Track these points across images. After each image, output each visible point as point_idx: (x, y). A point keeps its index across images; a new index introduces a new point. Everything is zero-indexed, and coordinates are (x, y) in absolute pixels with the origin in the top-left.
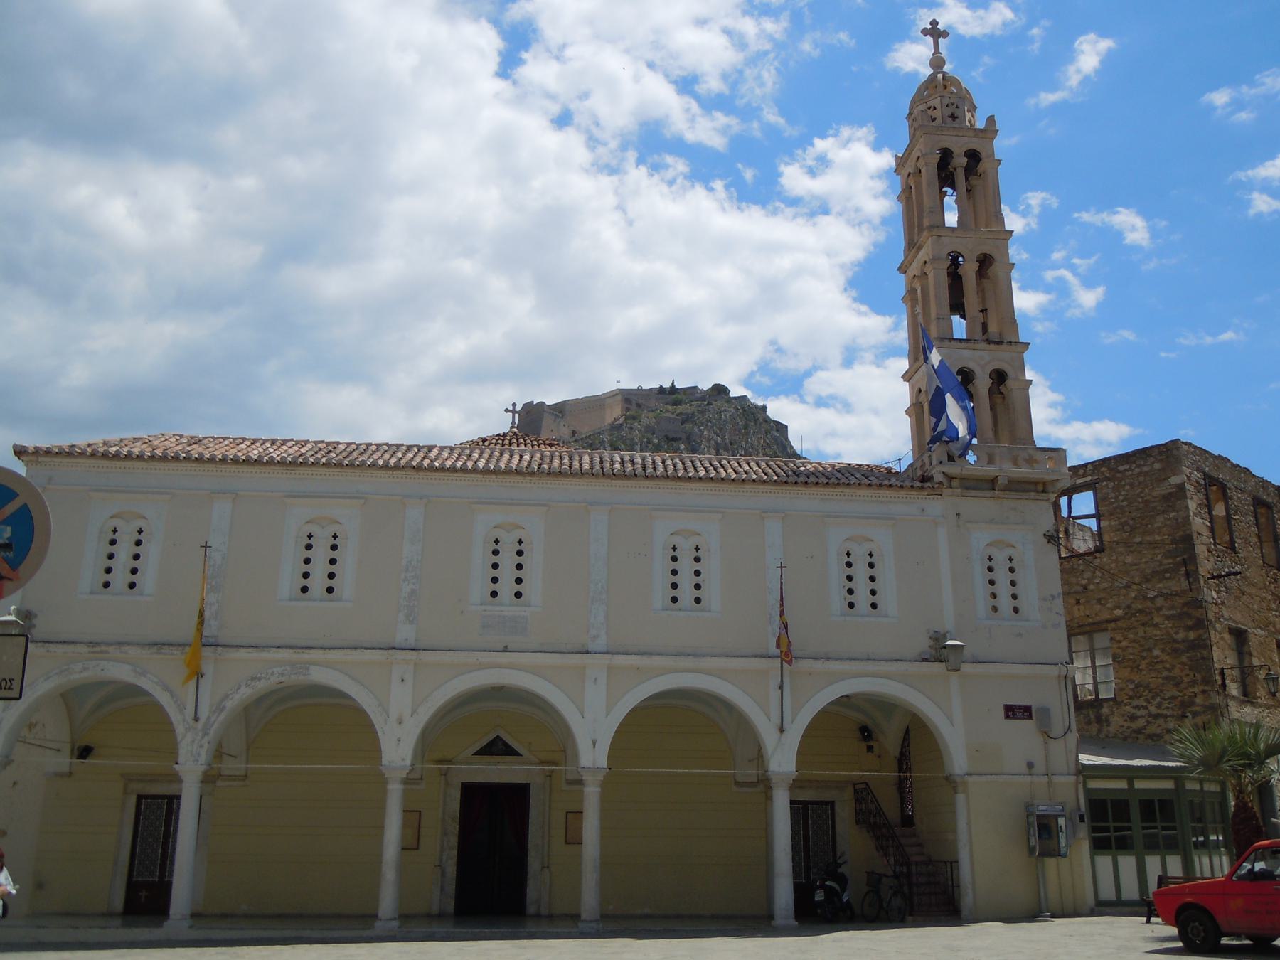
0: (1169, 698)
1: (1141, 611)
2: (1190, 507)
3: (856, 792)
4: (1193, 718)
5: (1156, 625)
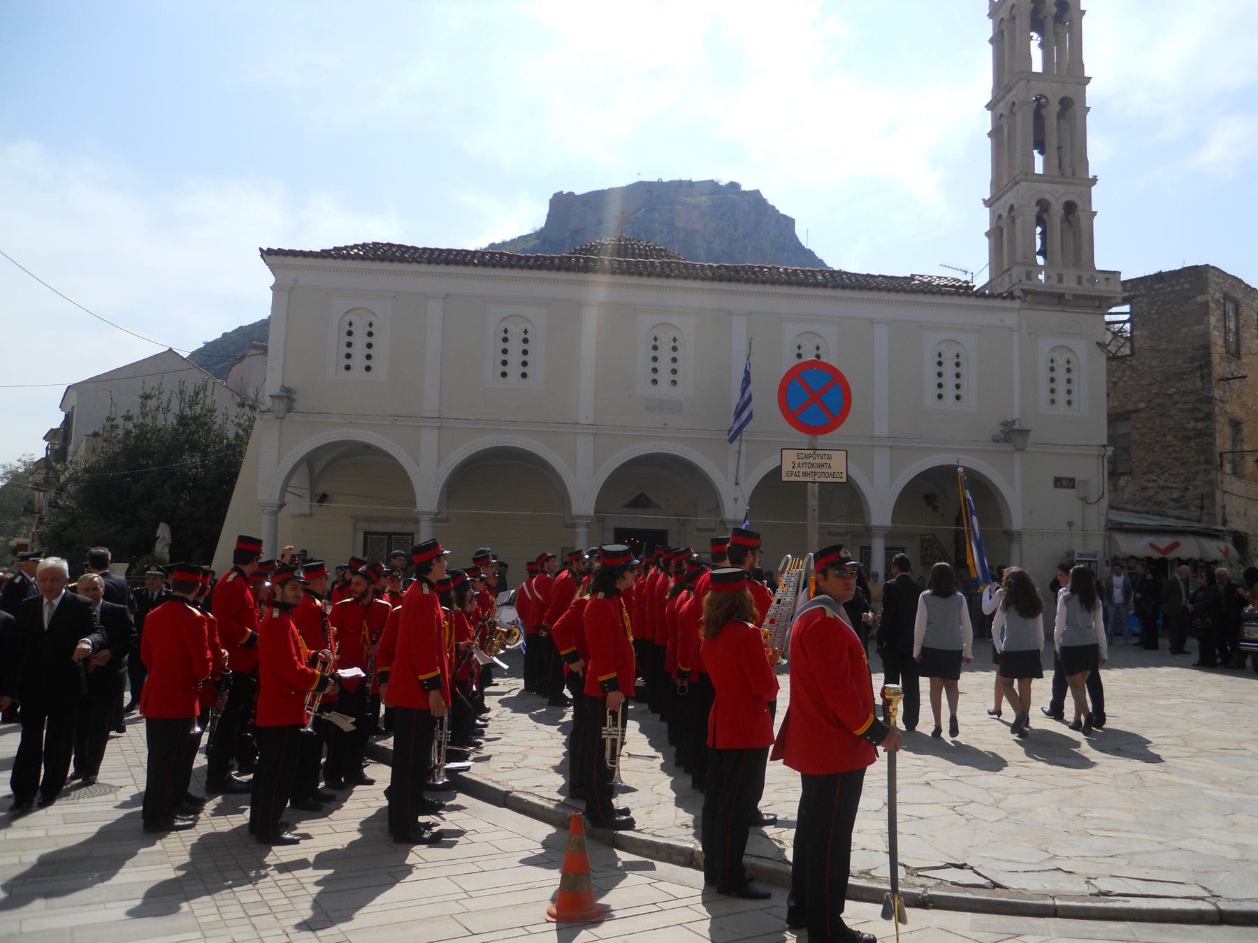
0: (1176, 475)
1: (1159, 405)
2: (1211, 322)
3: (922, 541)
5: (1172, 417)
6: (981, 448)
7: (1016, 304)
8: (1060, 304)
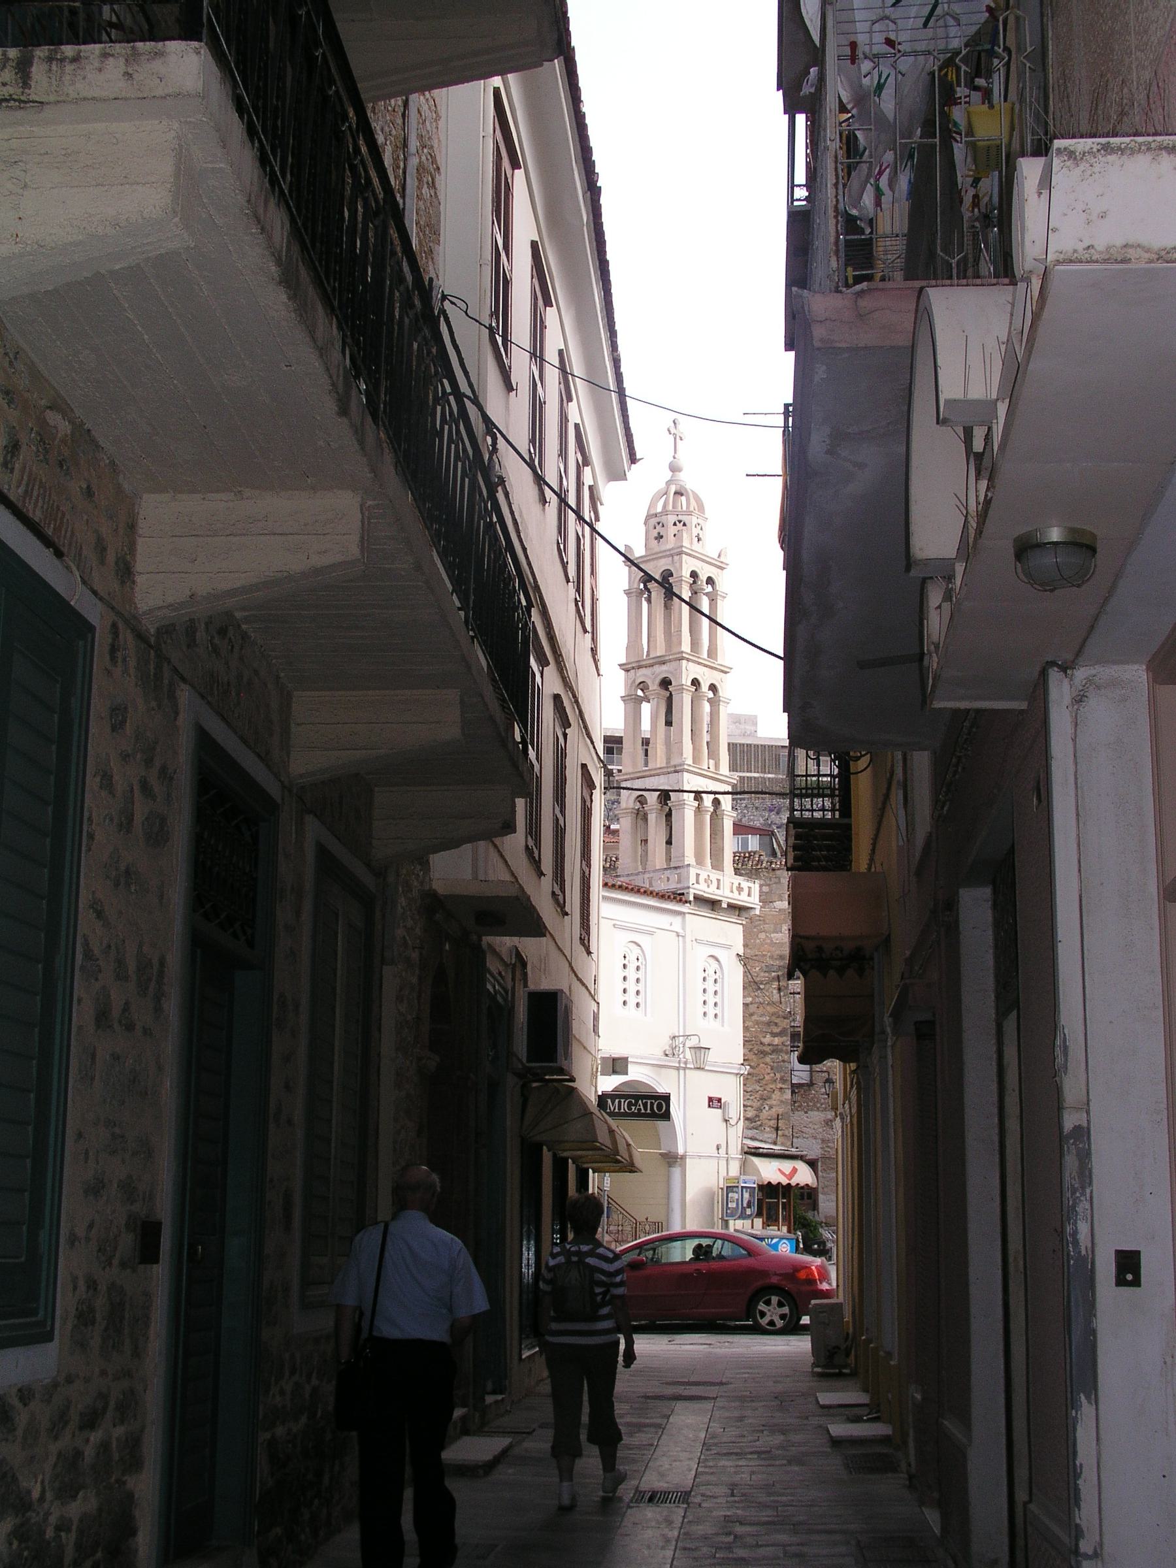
4: (769, 1109)
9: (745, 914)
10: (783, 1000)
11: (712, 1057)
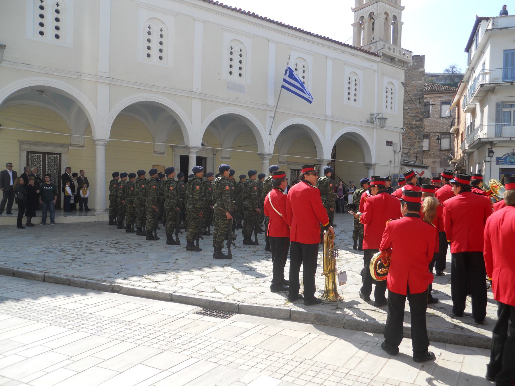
4: (414, 150)
6: (363, 125)
7: (378, 59)
8: (391, 62)
9: (405, 65)
10: (421, 107)
11: (388, 123)
